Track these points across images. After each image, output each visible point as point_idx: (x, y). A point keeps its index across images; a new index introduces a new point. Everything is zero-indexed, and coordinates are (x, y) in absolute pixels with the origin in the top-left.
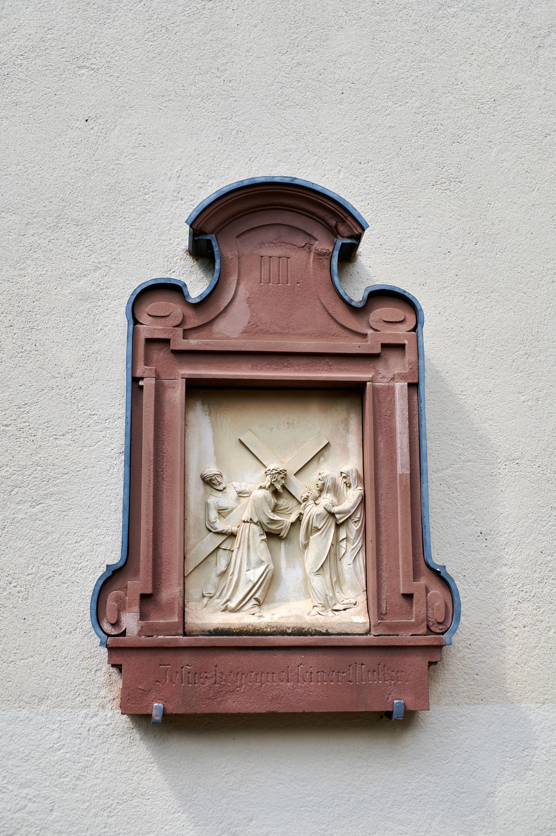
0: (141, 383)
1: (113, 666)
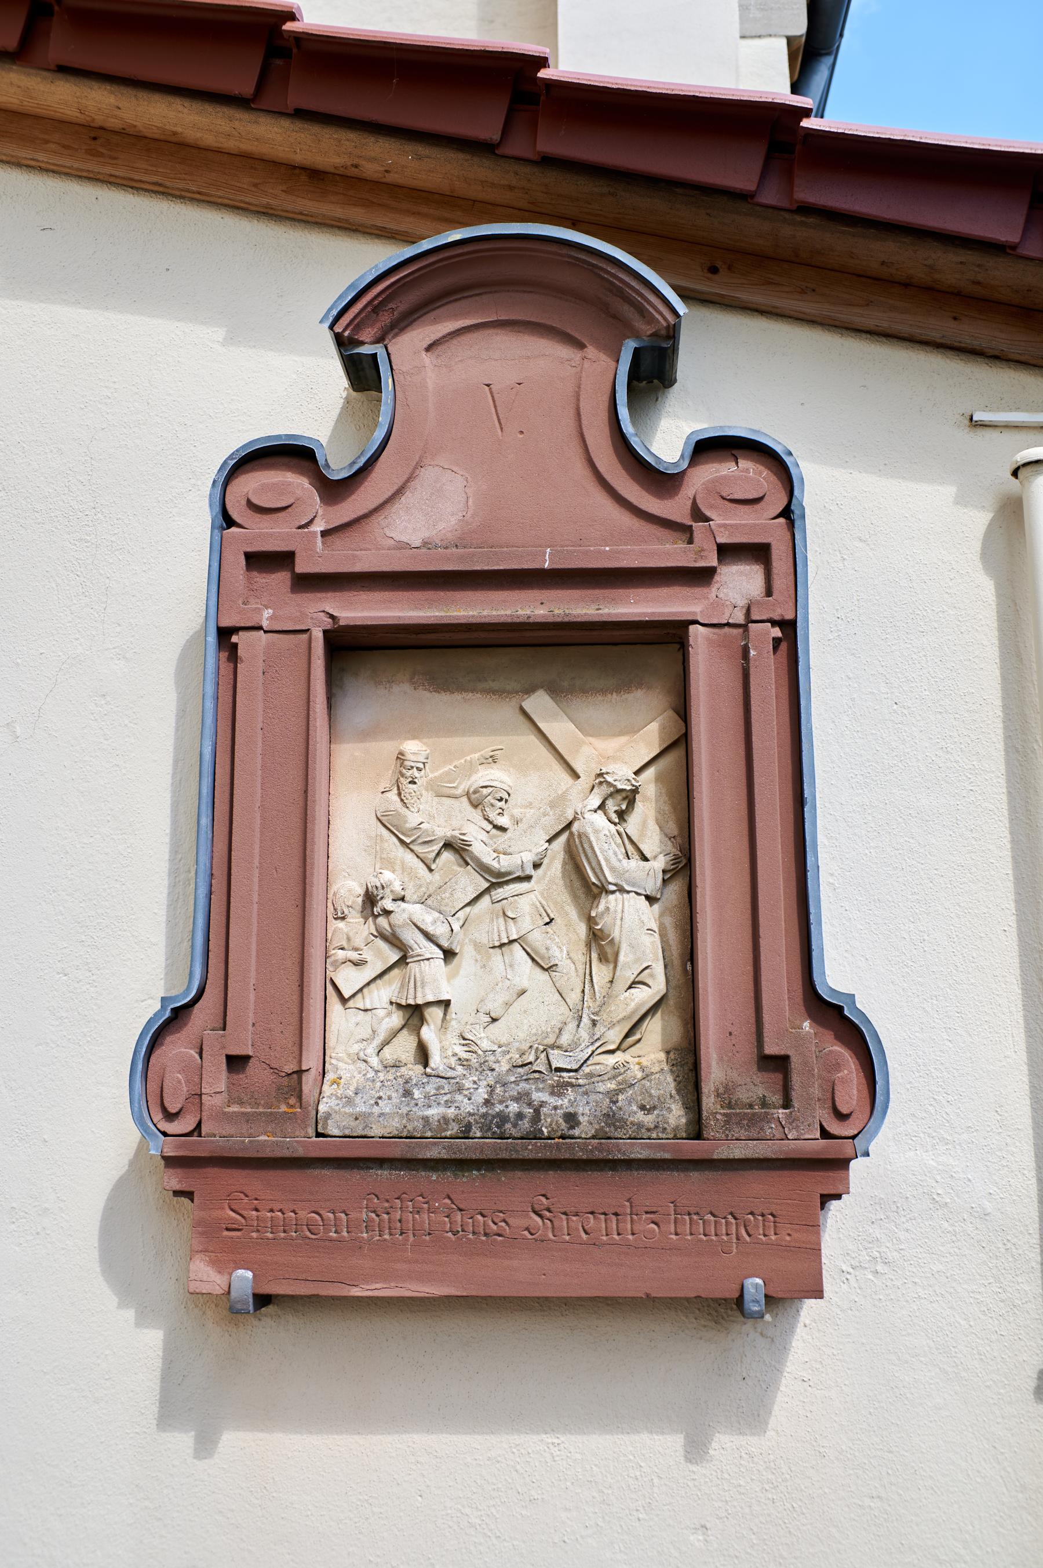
1: (177, 1193)
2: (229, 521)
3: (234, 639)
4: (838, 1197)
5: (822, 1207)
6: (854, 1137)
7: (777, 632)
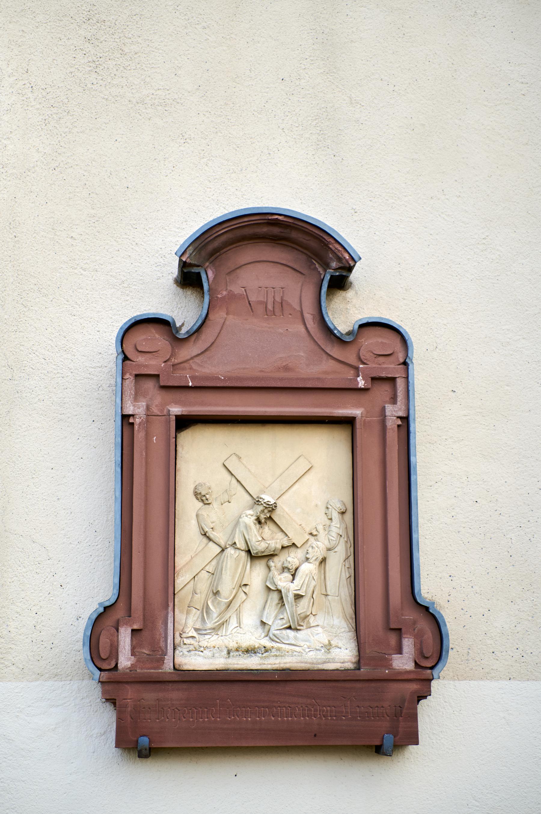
0: (131, 420)
3: (131, 420)
4: (425, 697)
5: (418, 704)
6: (432, 668)
7: (400, 422)
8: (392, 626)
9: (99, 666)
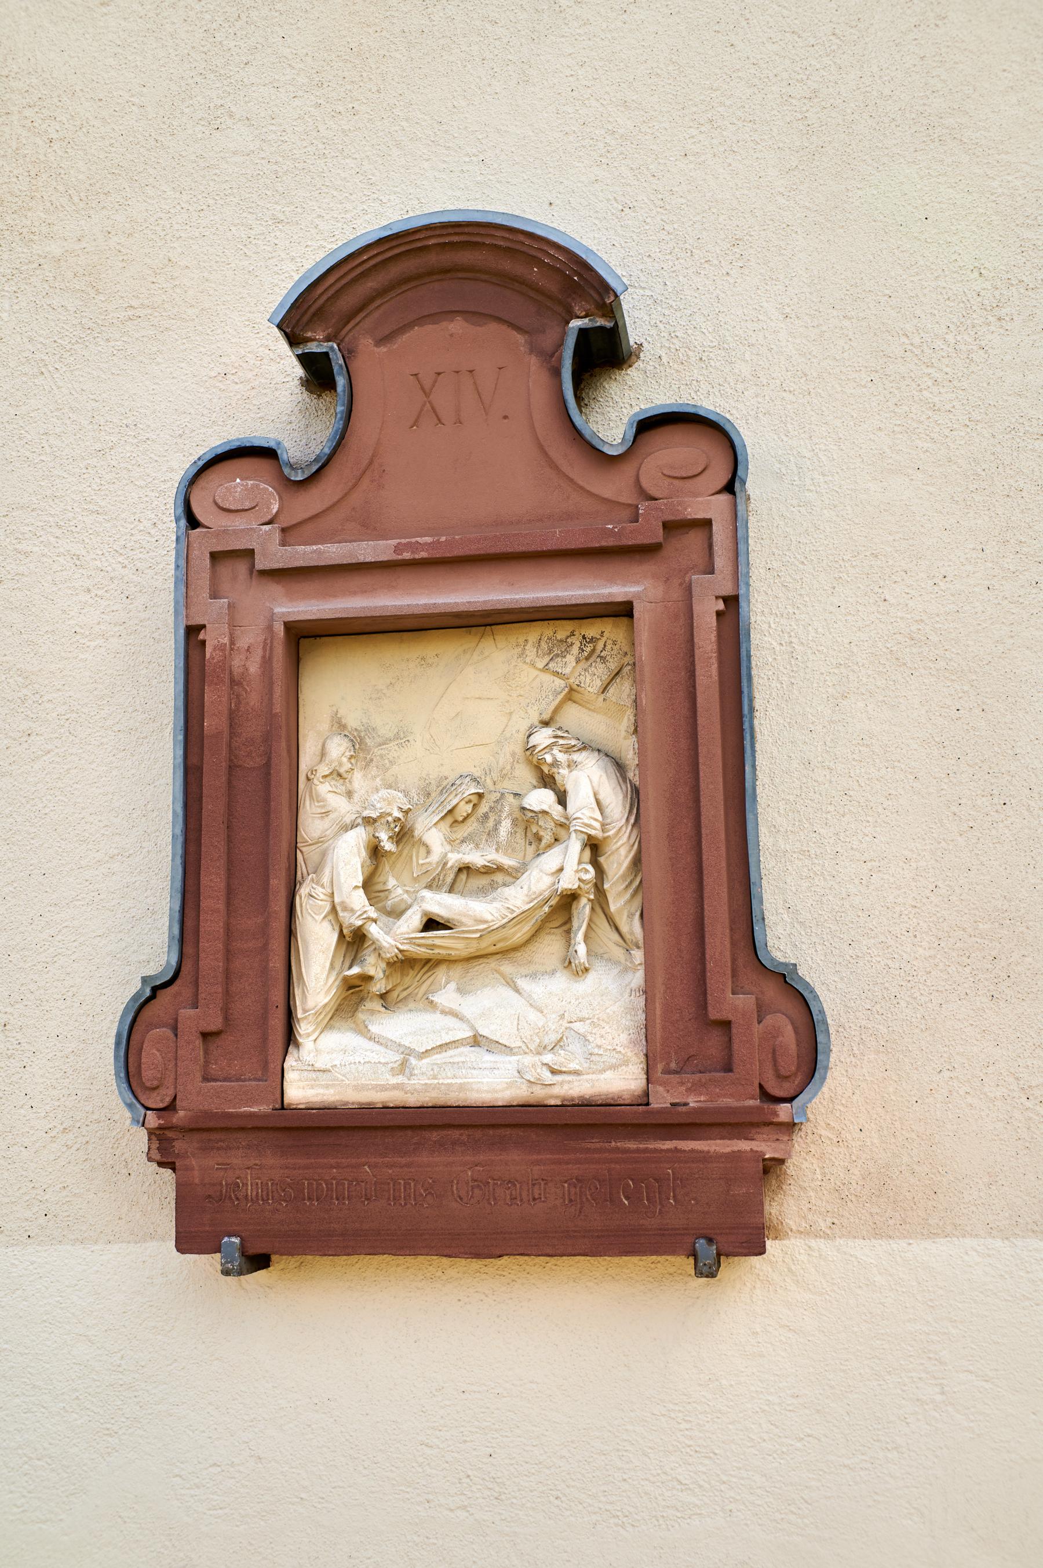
1: (161, 1164)
2: (193, 522)
3: (201, 637)
7: (721, 606)
8: (714, 1014)
9: (146, 1104)
